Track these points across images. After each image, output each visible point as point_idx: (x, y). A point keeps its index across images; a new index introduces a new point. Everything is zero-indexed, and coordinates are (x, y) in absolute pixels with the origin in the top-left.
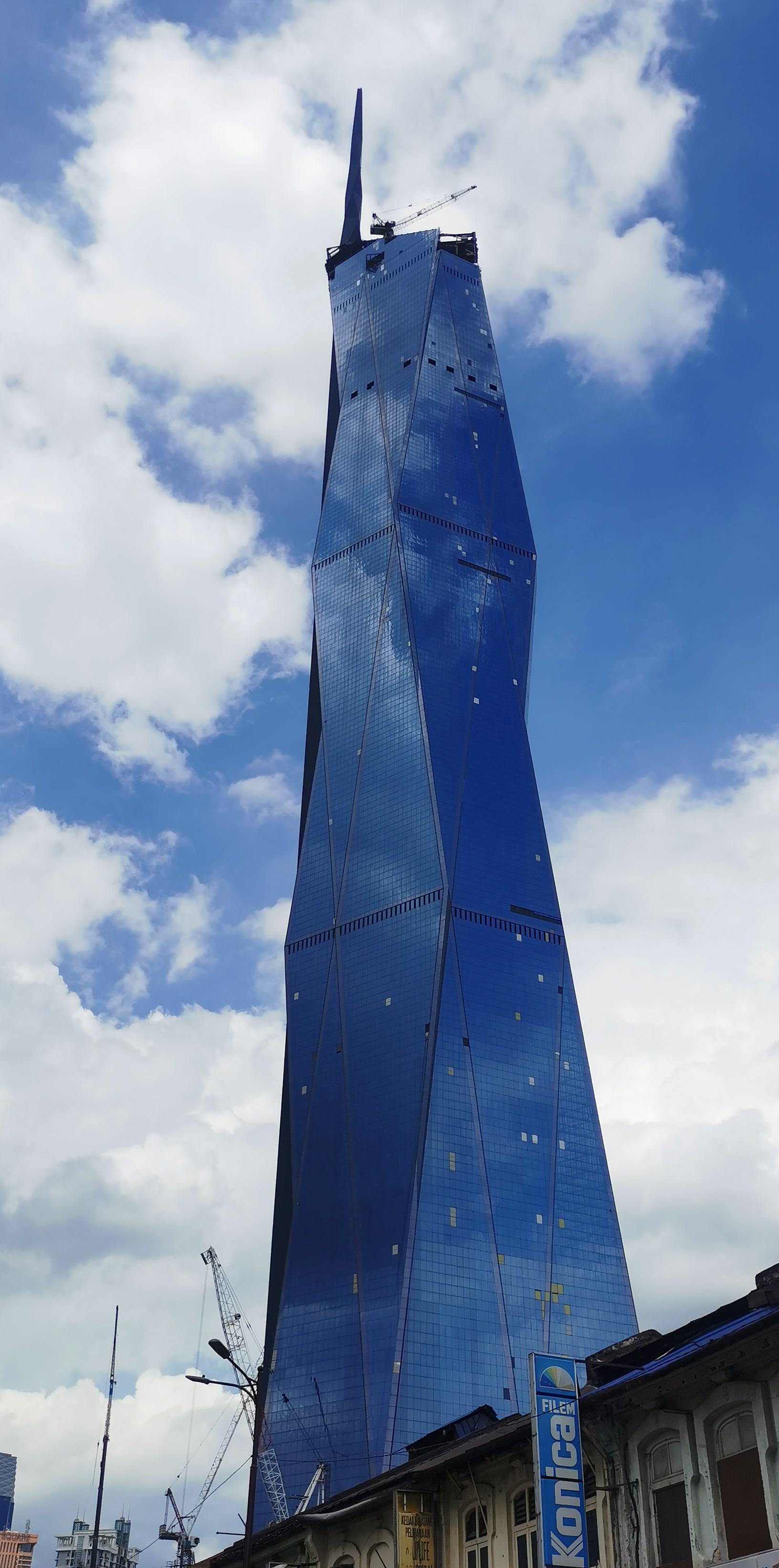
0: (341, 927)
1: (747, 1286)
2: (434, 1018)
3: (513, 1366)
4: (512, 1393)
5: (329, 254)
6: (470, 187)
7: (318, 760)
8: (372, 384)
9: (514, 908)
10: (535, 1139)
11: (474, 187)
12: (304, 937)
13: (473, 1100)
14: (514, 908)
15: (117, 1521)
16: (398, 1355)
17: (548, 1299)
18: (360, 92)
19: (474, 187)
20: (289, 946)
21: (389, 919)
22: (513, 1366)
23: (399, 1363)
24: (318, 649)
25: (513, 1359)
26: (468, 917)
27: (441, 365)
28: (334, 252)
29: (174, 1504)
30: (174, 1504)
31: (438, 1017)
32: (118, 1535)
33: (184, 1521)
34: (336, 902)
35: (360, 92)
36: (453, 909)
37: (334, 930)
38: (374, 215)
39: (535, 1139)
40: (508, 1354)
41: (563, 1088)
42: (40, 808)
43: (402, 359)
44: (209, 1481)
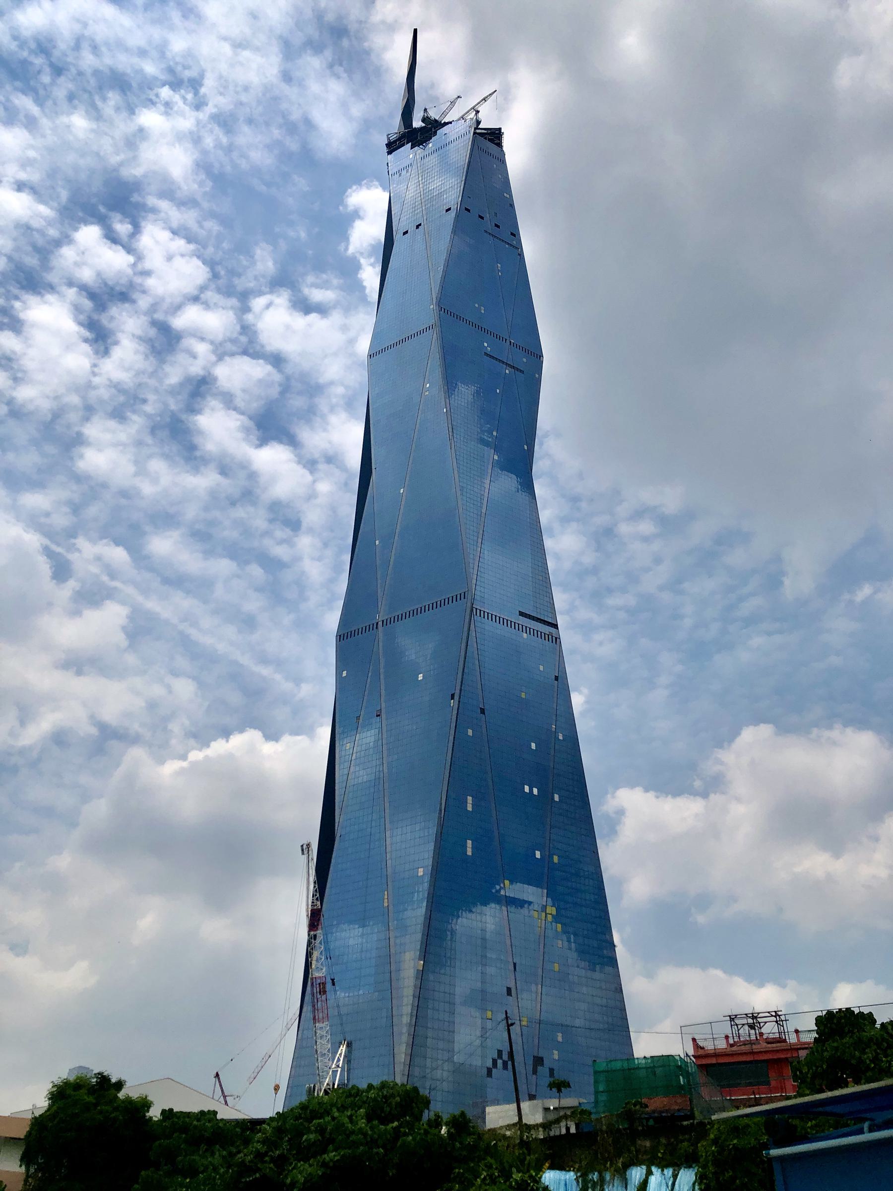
1: (42, 1103)
2: (458, 688)
4: (513, 992)
5: (389, 138)
8: (420, 225)
9: (522, 614)
10: (535, 791)
14: (522, 614)
18: (415, 31)
24: (337, 739)
25: (515, 964)
28: (393, 138)
29: (220, 1082)
30: (220, 1082)
31: (461, 690)
33: (228, 1098)
35: (415, 31)
38: (425, 110)
39: (535, 791)
40: (511, 960)
42: (215, 740)
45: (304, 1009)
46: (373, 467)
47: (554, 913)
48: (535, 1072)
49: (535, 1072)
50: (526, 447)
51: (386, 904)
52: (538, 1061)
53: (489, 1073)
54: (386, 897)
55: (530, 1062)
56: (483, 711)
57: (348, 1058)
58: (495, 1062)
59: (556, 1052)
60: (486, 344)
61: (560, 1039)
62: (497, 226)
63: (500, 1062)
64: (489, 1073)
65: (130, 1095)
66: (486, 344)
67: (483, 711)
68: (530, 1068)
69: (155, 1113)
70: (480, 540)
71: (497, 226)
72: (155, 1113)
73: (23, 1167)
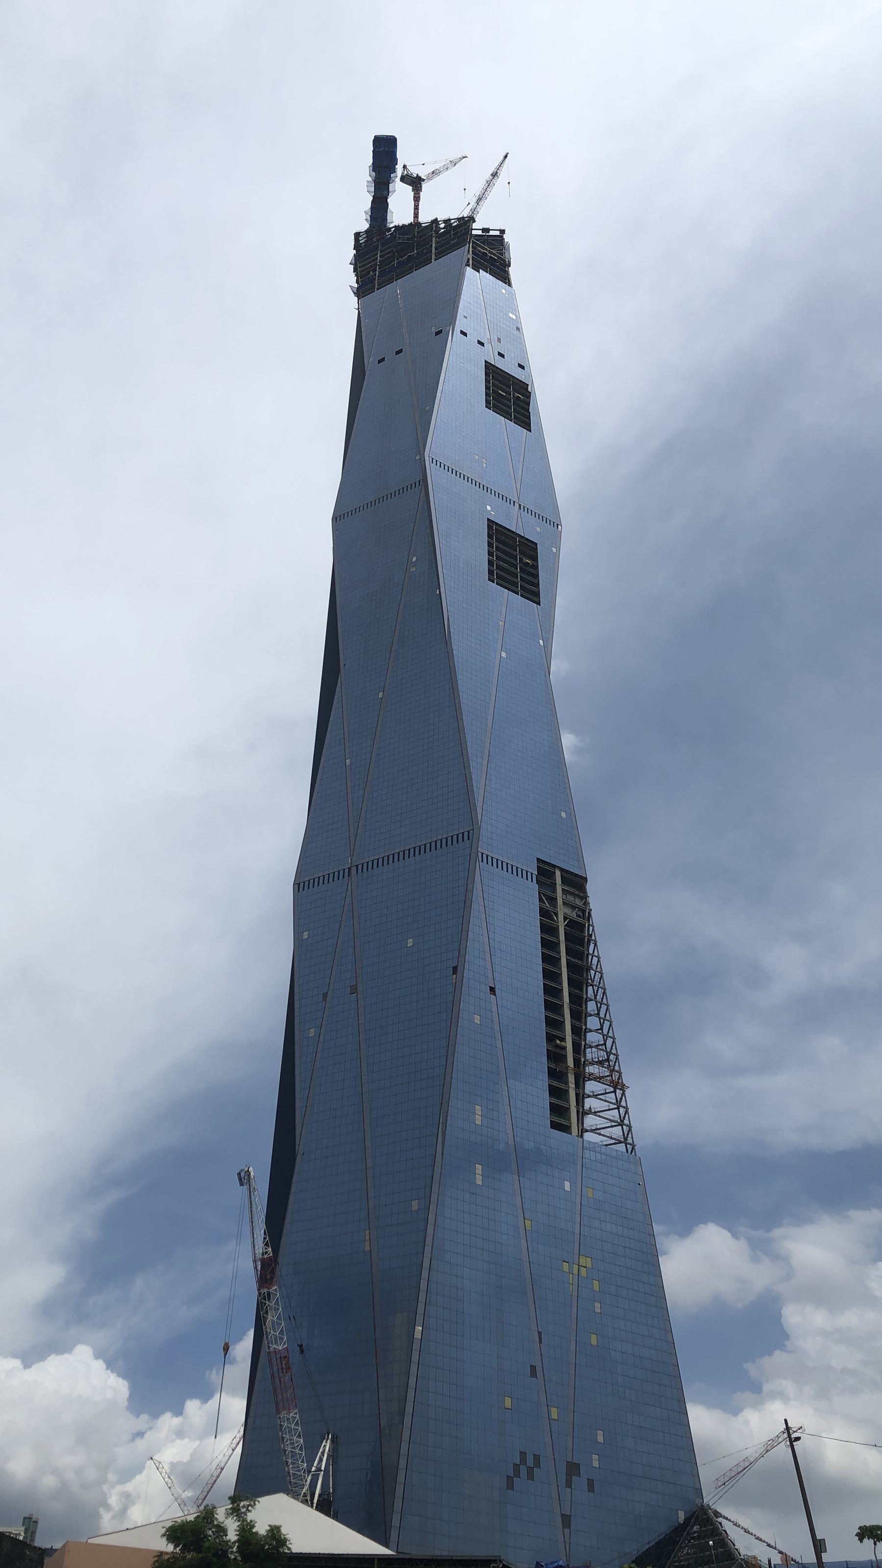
0: (357, 866)
3: (540, 1342)
6: (502, 158)
7: (336, 697)
11: (506, 157)
12: (316, 876)
13: (494, 1009)
15: (25, 1518)
16: (419, 1318)
17: (575, 1271)
19: (506, 157)
20: (299, 885)
21: (412, 858)
22: (540, 1342)
23: (421, 1328)
25: (540, 1333)
26: (495, 863)
27: (472, 338)
32: (25, 1533)
34: (352, 841)
36: (480, 855)
37: (350, 869)
41: (587, 1154)
43: (433, 329)
44: (211, 1482)
45: (259, 1375)
46: (342, 664)
47: (589, 1265)
48: (569, 1484)
49: (569, 1484)
50: (541, 642)
51: (367, 1249)
52: (573, 1469)
53: (510, 1485)
54: (367, 1238)
55: (563, 1468)
56: (492, 990)
57: (334, 1456)
58: (516, 1468)
59: (595, 1457)
60: (489, 508)
61: (600, 1439)
62: (500, 354)
63: (523, 1470)
64: (510, 1485)
65: (284, 1531)
66: (489, 508)
67: (492, 990)
68: (563, 1478)
69: (254, 1530)
70: (485, 762)
71: (500, 354)
72: (254, 1530)
73: (261, 1529)
